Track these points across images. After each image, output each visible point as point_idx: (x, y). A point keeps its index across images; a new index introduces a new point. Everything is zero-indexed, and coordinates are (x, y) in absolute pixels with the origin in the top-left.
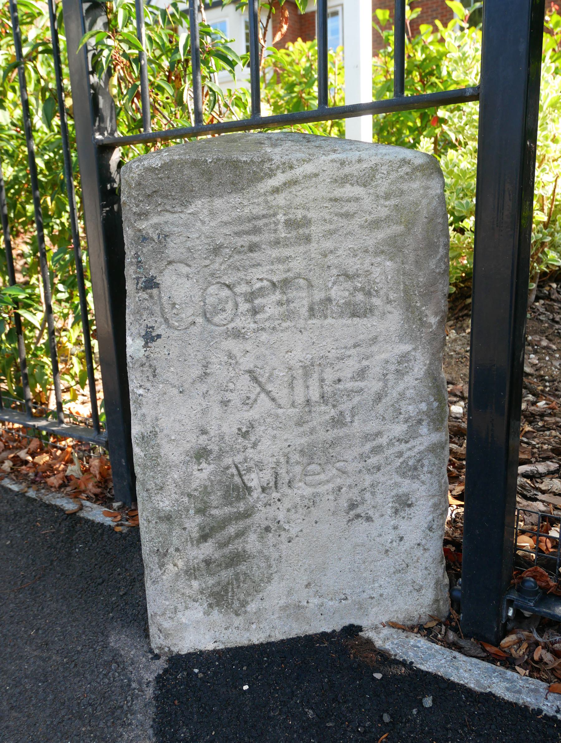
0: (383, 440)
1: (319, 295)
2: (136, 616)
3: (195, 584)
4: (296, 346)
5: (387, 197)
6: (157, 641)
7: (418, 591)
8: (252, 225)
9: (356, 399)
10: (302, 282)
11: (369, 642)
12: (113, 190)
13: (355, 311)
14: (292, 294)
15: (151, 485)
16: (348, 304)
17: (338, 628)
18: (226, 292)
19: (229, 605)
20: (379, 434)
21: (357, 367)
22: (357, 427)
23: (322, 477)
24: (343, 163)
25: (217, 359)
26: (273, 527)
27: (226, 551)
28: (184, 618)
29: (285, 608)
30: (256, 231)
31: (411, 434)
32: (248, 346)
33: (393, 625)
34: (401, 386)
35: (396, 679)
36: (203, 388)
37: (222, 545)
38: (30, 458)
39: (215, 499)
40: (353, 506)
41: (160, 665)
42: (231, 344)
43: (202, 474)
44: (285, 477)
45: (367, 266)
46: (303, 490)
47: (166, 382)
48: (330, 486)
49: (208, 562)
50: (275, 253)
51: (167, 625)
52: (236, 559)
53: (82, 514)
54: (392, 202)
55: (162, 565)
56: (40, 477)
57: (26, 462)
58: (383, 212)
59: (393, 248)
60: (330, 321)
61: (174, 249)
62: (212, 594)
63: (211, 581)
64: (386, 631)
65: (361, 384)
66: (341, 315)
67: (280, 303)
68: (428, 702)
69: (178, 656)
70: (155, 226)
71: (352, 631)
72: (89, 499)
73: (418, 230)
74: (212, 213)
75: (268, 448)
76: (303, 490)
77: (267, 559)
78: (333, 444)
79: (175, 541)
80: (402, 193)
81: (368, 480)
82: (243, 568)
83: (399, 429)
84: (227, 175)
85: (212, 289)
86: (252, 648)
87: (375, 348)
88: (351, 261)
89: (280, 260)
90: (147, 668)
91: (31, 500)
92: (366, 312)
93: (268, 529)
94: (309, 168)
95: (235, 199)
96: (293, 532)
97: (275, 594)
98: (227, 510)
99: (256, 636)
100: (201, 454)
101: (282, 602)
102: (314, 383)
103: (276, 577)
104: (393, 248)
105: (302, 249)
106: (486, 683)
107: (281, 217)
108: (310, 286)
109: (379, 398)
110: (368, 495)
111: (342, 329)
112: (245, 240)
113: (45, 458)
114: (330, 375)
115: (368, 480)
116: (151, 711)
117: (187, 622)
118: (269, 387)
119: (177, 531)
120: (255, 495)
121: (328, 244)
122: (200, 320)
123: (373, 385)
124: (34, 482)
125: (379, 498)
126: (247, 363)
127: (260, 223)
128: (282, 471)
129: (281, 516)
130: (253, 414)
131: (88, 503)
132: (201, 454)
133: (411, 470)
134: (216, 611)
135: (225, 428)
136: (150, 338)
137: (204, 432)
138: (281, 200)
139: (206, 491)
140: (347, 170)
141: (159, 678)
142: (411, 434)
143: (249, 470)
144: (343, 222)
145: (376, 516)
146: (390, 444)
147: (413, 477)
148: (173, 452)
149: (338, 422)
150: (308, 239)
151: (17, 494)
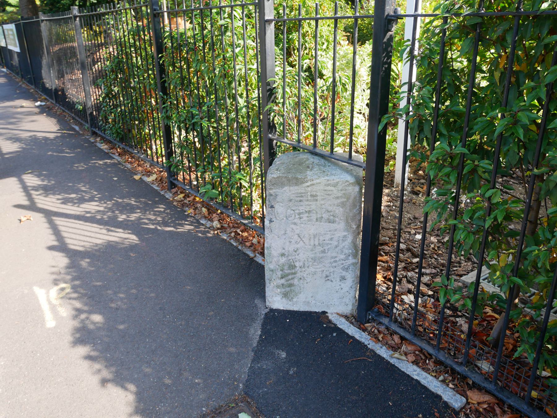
0: (337, 259)
1: (319, 216)
2: (262, 295)
3: (279, 290)
4: (312, 229)
5: (341, 190)
6: (267, 304)
7: (347, 305)
8: (301, 195)
9: (329, 246)
10: (314, 212)
11: (328, 317)
12: (274, 152)
13: (330, 222)
14: (311, 215)
15: (268, 261)
16: (328, 219)
17: (320, 311)
18: (292, 212)
19: (288, 298)
20: (336, 257)
21: (330, 237)
22: (329, 254)
23: (318, 267)
24: (328, 180)
25: (289, 230)
26: (302, 278)
27: (288, 282)
28: (275, 299)
29: (304, 302)
30: (302, 196)
31: (346, 259)
32: (298, 227)
33: (338, 314)
34: (344, 244)
35: (330, 327)
36: (285, 237)
37: (287, 281)
38: (241, 233)
39: (286, 267)
40: (327, 276)
41: (268, 310)
42: (293, 226)
43: (283, 260)
44: (306, 265)
45: (334, 209)
46: (312, 269)
47: (274, 234)
48: (320, 270)
49: (283, 285)
50: (307, 203)
51: (270, 300)
52: (291, 285)
53: (255, 259)
54: (343, 192)
55: (270, 283)
56: (243, 241)
57: (239, 234)
58: (340, 195)
59: (343, 205)
60: (322, 223)
61: (279, 199)
62: (283, 294)
63: (283, 290)
64: (334, 315)
65: (331, 242)
66: (326, 222)
67: (308, 217)
68: (335, 334)
69: (273, 309)
70: (274, 192)
71: (324, 313)
72: (258, 253)
73: (351, 201)
74: (290, 191)
75: (302, 256)
76: (312, 269)
77: (300, 287)
78: (321, 258)
79: (274, 277)
80: (346, 190)
81: (332, 270)
82: (293, 288)
83: (343, 257)
84: (295, 181)
85: (289, 211)
86: (294, 311)
87: (336, 233)
88: (329, 207)
89: (308, 205)
90: (263, 310)
91: (239, 250)
92: (334, 222)
93: (301, 279)
94: (318, 181)
95: (296, 188)
96: (308, 281)
97: (302, 297)
98: (289, 271)
99: (295, 309)
100: (283, 255)
101: (304, 300)
102: (317, 240)
103: (302, 293)
104: (343, 205)
105: (315, 203)
106: (354, 334)
107: (309, 194)
108: (317, 213)
109: (336, 247)
110: (332, 274)
111: (324, 227)
112: (299, 199)
113: (245, 234)
114: (322, 238)
115: (332, 270)
116: (262, 321)
117: (276, 301)
118: (303, 239)
119: (275, 274)
120: (297, 268)
121: (323, 202)
122: (285, 218)
123: (335, 243)
124: (241, 243)
125: (335, 276)
126: (297, 232)
127: (303, 195)
128: (306, 263)
129: (305, 276)
130: (298, 246)
131: (258, 255)
132: (283, 255)
133: (346, 269)
134: (284, 299)
135: (290, 249)
136: (271, 221)
137: (284, 249)
138: (309, 189)
139: (283, 265)
140: (329, 182)
141: (266, 313)
142: (346, 259)
143: (296, 261)
144: (328, 196)
145: (334, 281)
146: (339, 260)
147: (346, 271)
148: (275, 253)
149: (323, 252)
150: (317, 200)
151: (235, 247)
